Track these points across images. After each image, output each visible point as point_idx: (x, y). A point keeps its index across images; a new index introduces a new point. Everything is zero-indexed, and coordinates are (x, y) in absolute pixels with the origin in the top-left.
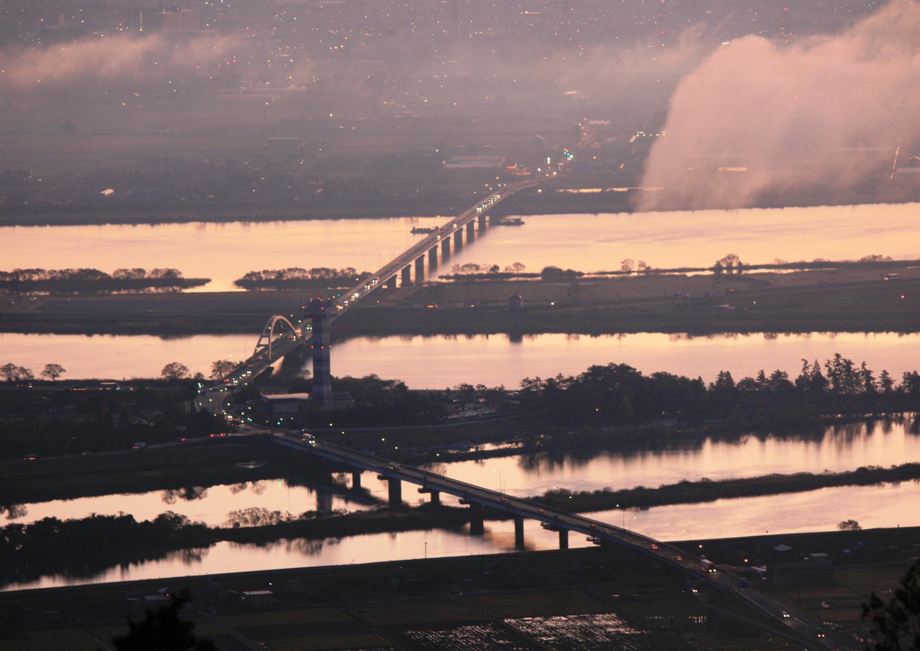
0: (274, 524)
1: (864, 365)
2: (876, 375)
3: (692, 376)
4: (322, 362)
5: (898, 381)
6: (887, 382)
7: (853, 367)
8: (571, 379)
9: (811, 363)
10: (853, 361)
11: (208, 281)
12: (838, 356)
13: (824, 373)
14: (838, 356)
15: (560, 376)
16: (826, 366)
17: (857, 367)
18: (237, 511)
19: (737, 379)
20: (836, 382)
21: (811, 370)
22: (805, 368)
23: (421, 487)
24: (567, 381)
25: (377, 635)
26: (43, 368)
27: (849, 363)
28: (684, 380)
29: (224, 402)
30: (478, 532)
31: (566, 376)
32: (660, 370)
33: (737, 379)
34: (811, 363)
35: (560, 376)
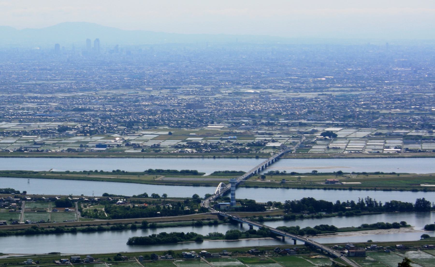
0: (312, 113)
1: (375, 199)
2: (378, 202)
3: (329, 201)
4: (233, 194)
5: (383, 204)
6: (381, 204)
7: (372, 200)
8: (298, 201)
9: (361, 198)
10: (372, 198)
11: (205, 173)
12: (368, 197)
13: (364, 201)
14: (368, 197)
15: (295, 200)
16: (365, 199)
17: (373, 200)
18: (21, 192)
19: (341, 202)
20: (367, 204)
21: (361, 201)
22: (359, 200)
23: (383, 205)
24: (297, 201)
25: (159, 152)
26: (162, 195)
27: (371, 199)
28: (327, 202)
29: (171, 127)
30: (307, 244)
31: (297, 200)
32: (321, 199)
33: (341, 202)
34: (361, 198)
35: (295, 200)
